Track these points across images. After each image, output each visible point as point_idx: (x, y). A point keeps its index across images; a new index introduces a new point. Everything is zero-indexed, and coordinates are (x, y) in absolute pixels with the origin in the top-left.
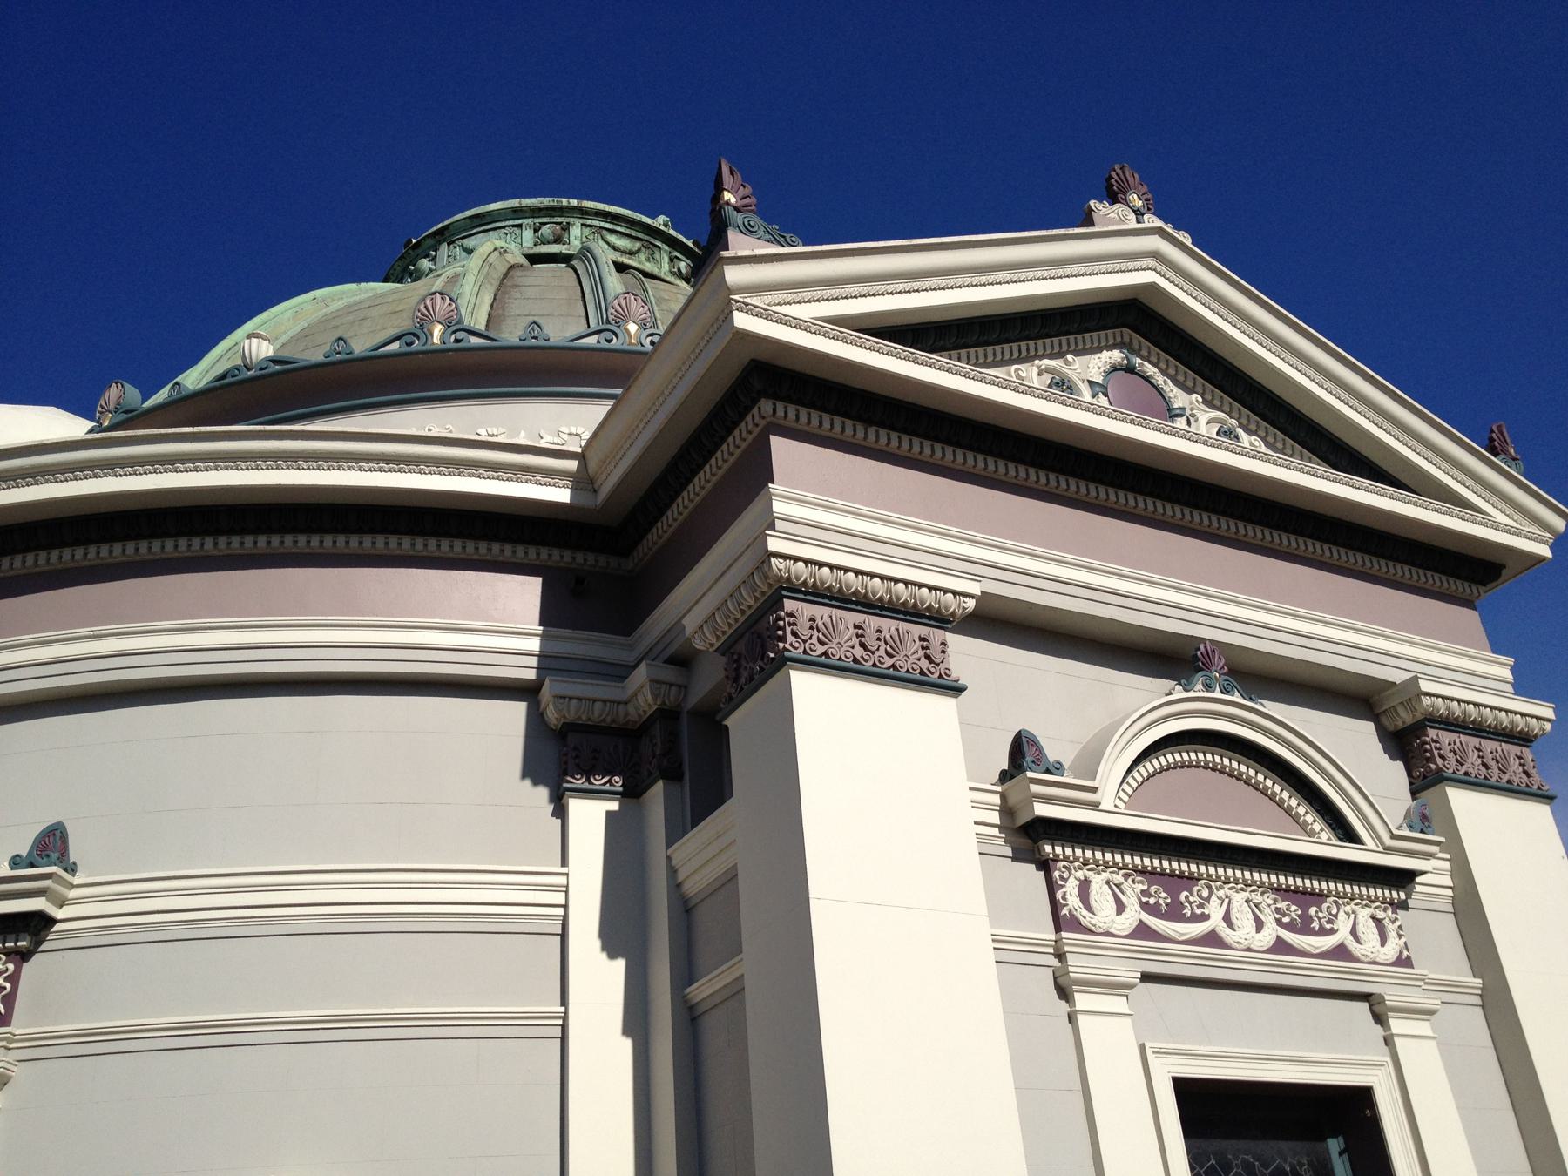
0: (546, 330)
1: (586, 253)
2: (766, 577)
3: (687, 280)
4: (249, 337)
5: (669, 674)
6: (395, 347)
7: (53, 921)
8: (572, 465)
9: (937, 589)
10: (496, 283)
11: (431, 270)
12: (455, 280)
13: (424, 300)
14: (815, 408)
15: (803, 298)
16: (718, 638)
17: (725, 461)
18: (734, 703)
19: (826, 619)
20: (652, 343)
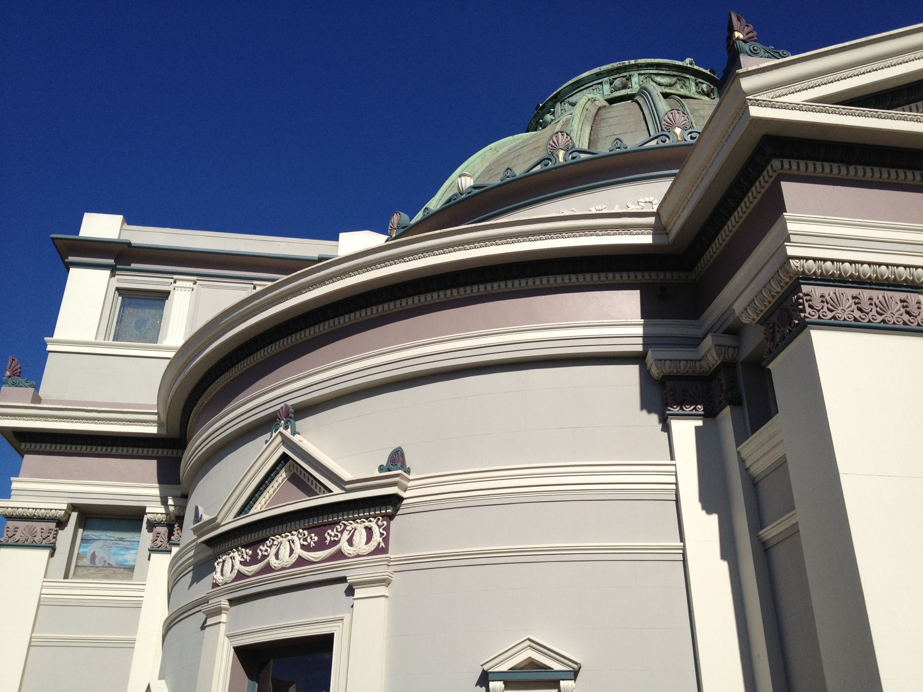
0: (624, 142)
1: (643, 91)
2: (788, 272)
3: (708, 95)
4: (460, 177)
5: (726, 340)
6: (538, 168)
7: (401, 499)
8: (651, 220)
9: (910, 267)
10: (591, 120)
11: (552, 120)
12: (567, 122)
13: (552, 138)
14: (810, 159)
15: (791, 90)
16: (758, 314)
17: (751, 203)
18: (773, 354)
19: (831, 294)
20: (692, 138)
